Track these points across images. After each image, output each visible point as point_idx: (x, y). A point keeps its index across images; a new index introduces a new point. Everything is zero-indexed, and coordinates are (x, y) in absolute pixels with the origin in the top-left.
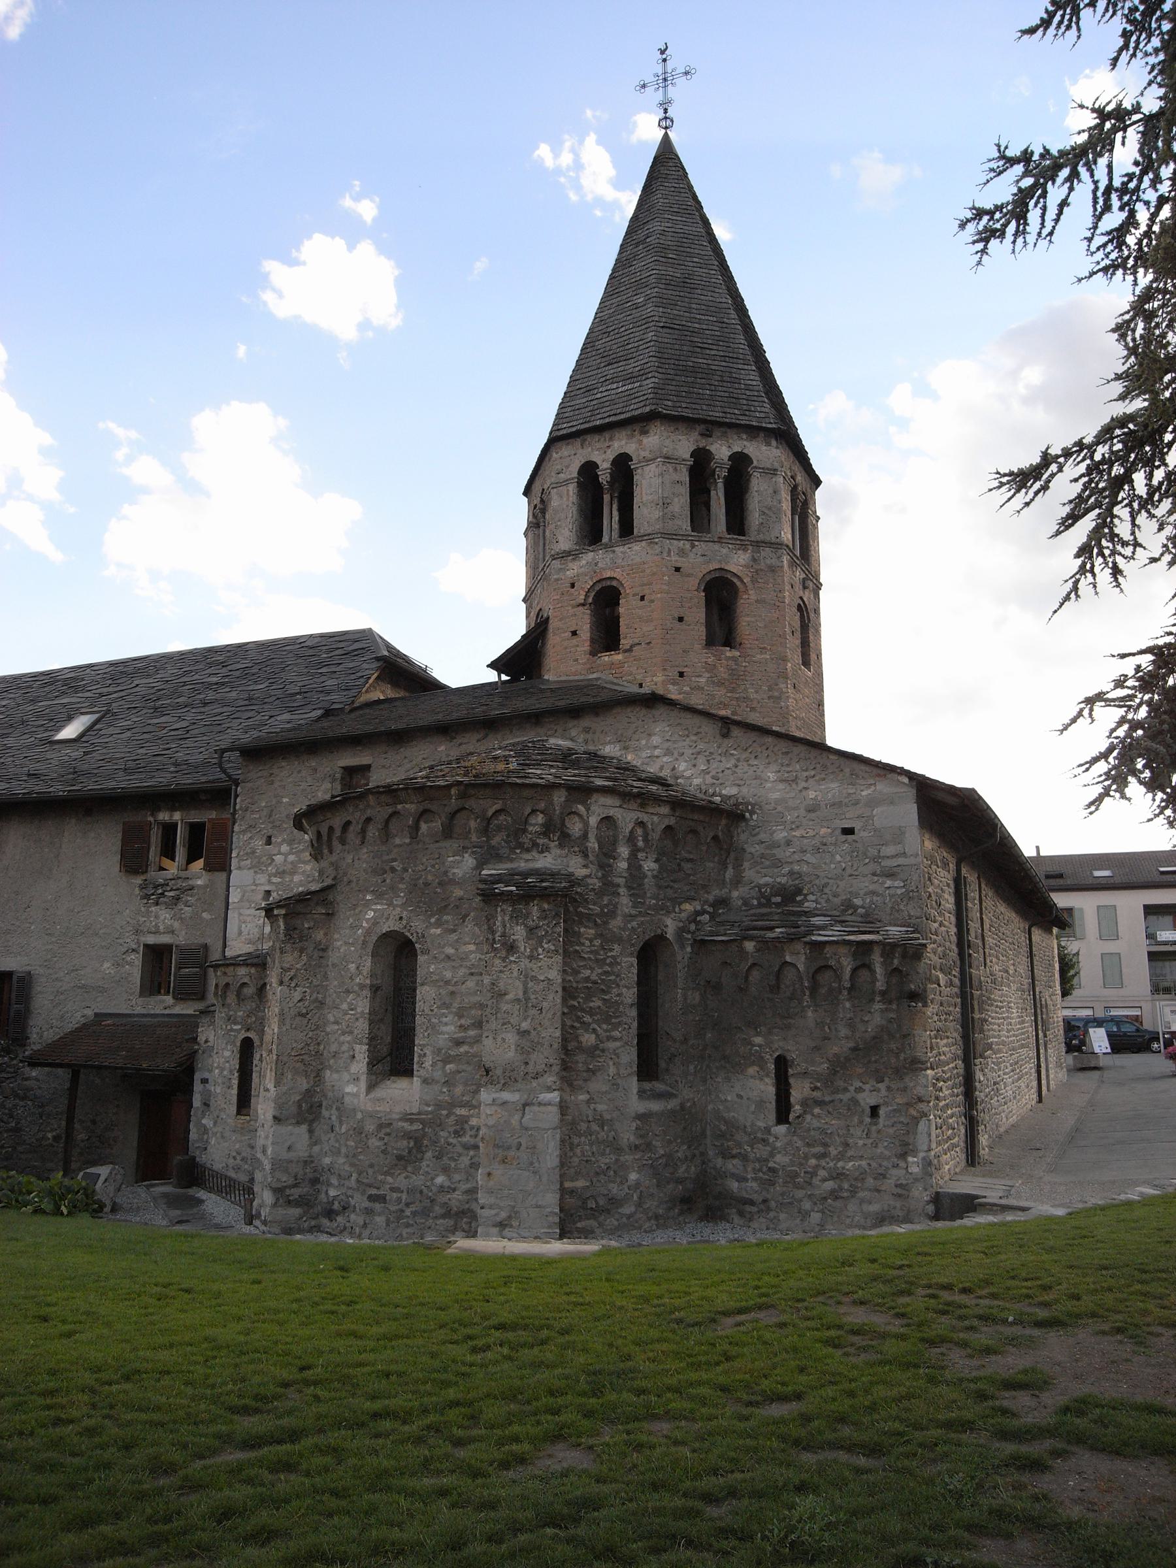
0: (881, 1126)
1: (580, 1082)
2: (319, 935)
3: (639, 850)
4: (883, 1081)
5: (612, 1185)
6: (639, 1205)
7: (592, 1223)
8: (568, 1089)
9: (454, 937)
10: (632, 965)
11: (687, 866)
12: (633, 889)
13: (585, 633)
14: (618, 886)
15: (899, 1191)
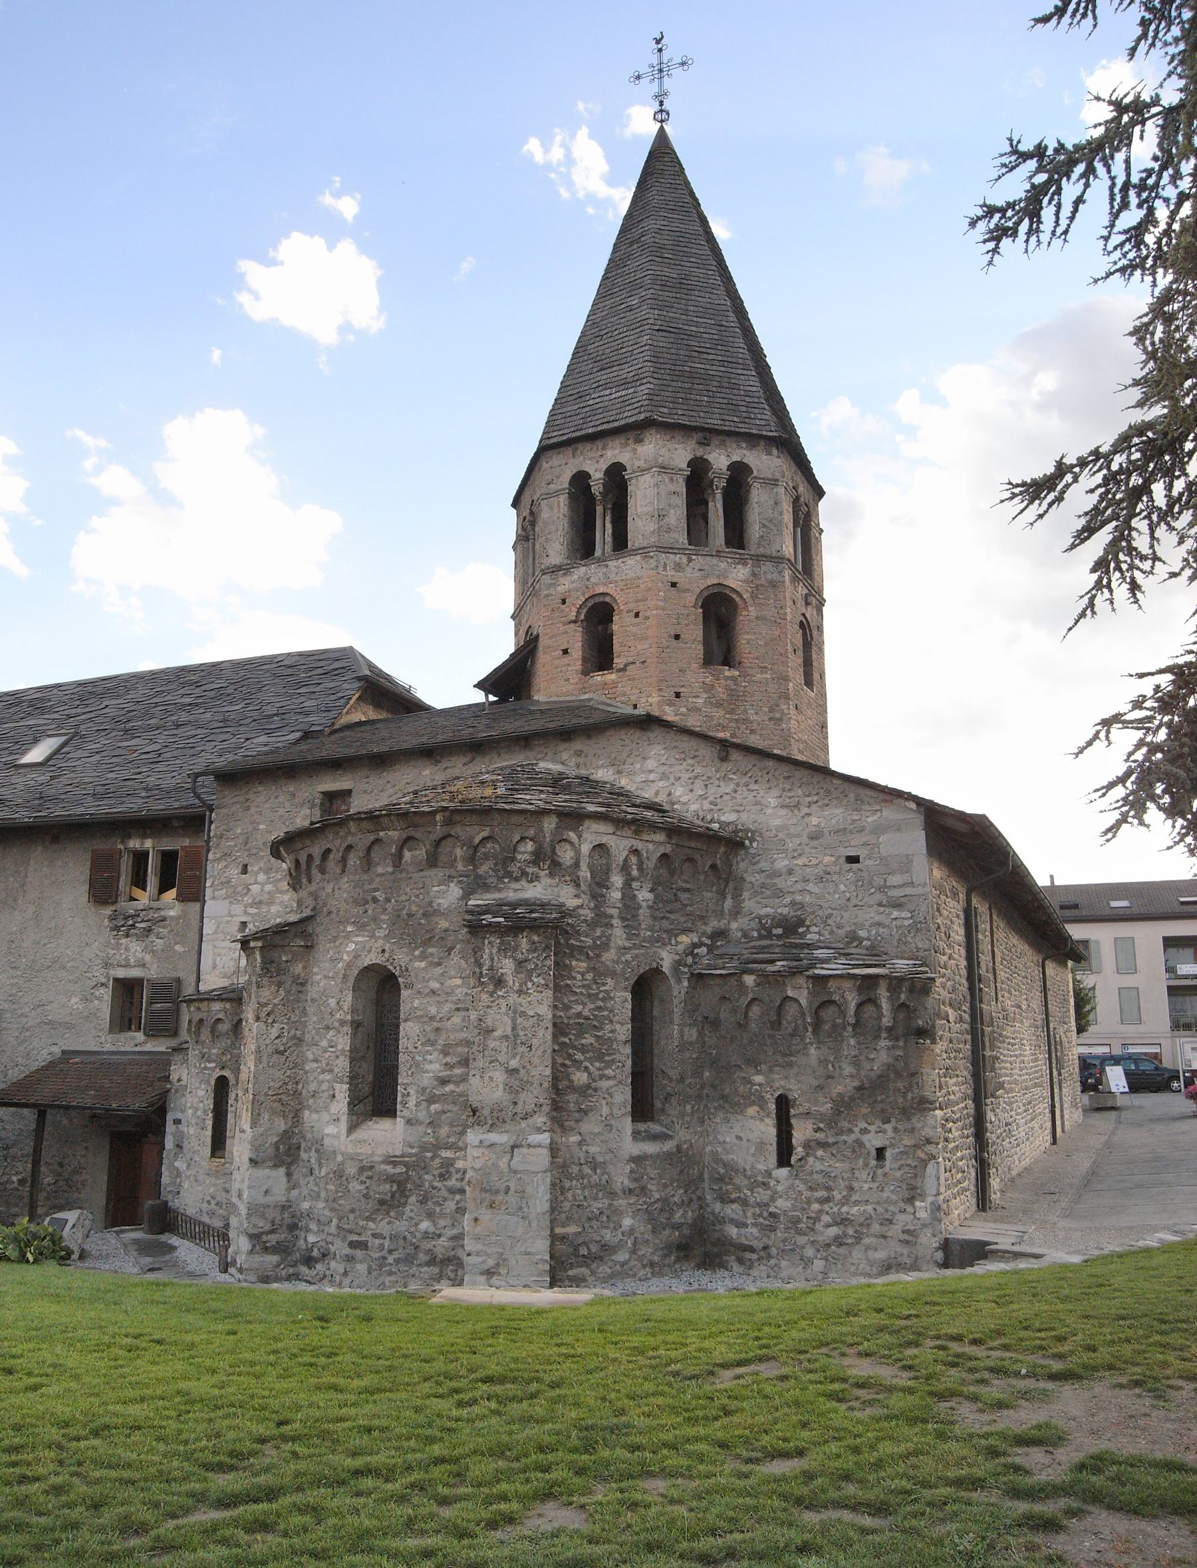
1: (572, 1123)
2: (298, 968)
3: (633, 880)
4: (889, 1122)
6: (633, 1252)
7: (584, 1271)
9: (439, 970)
10: (626, 1000)
11: (684, 896)
12: (627, 920)
13: (577, 652)
14: (612, 917)
15: (906, 1237)
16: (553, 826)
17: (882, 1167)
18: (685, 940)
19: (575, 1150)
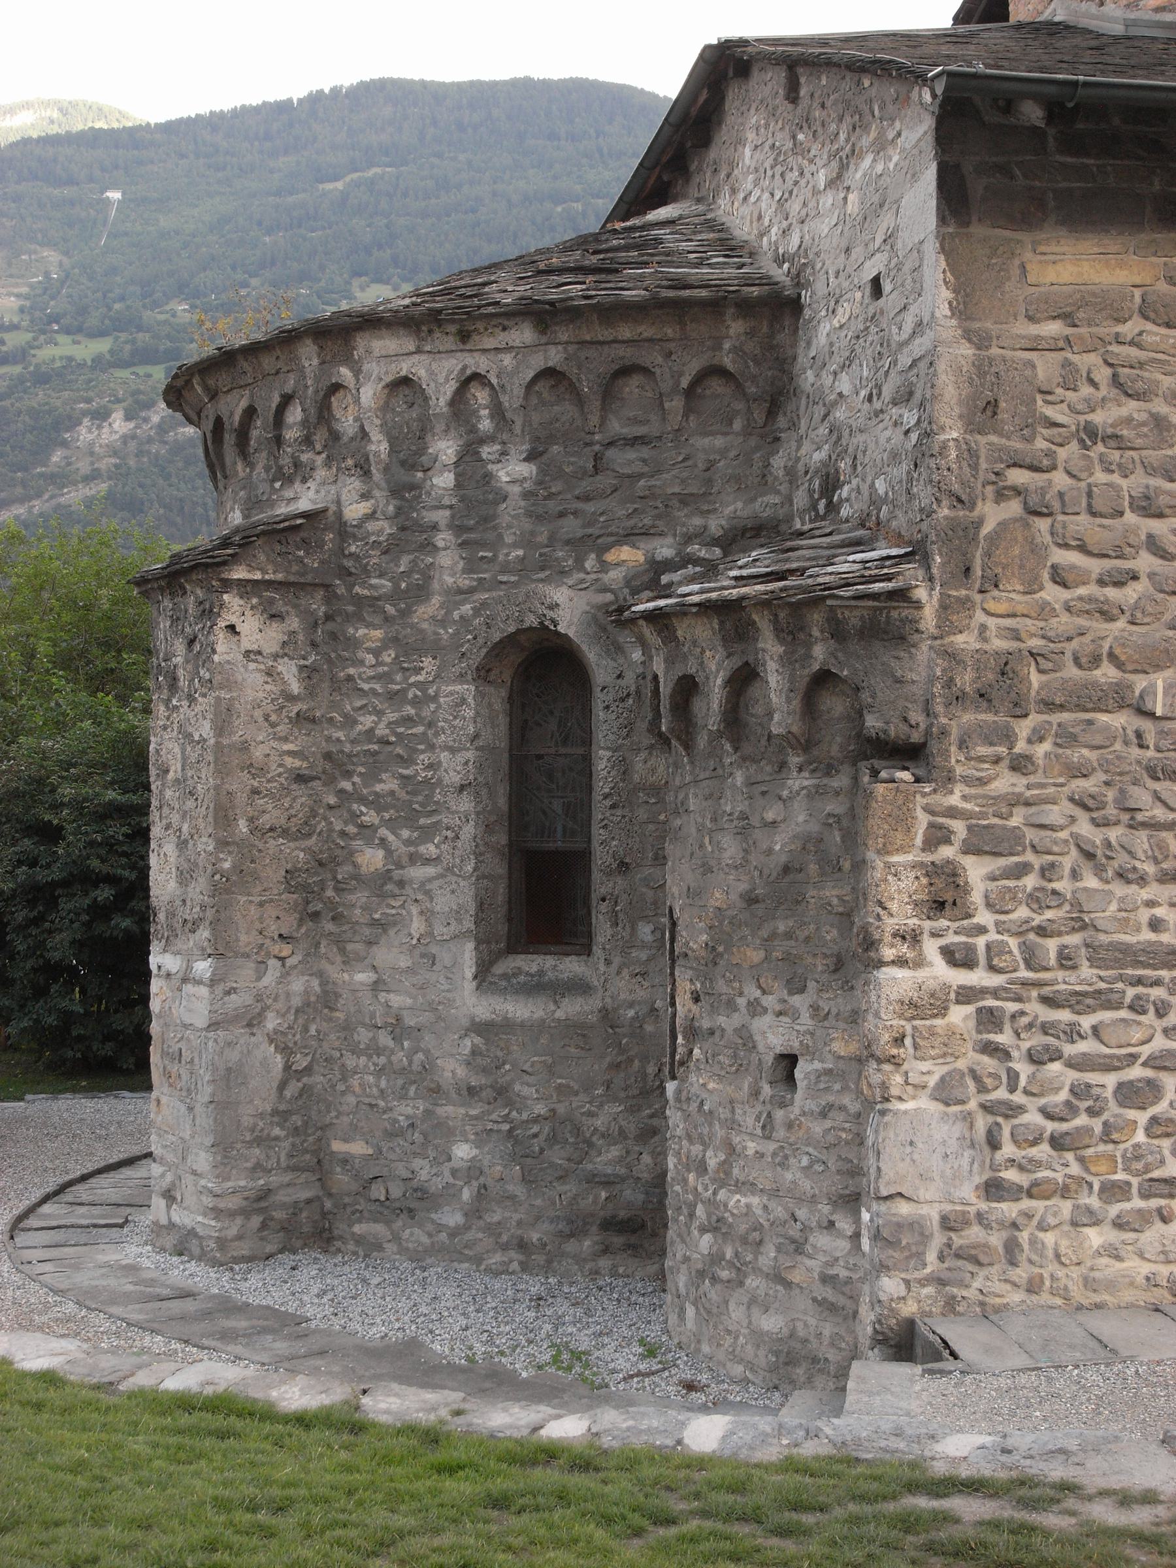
0: (796, 1110)
1: (359, 947)
3: (482, 441)
4: (802, 990)
5: (417, 1163)
6: (474, 1213)
7: (379, 1229)
8: (339, 959)
10: (463, 701)
11: (624, 460)
12: (470, 529)
14: (435, 527)
15: (828, 1293)
16: (315, 362)
17: (783, 1105)
18: (629, 555)
19: (366, 998)
